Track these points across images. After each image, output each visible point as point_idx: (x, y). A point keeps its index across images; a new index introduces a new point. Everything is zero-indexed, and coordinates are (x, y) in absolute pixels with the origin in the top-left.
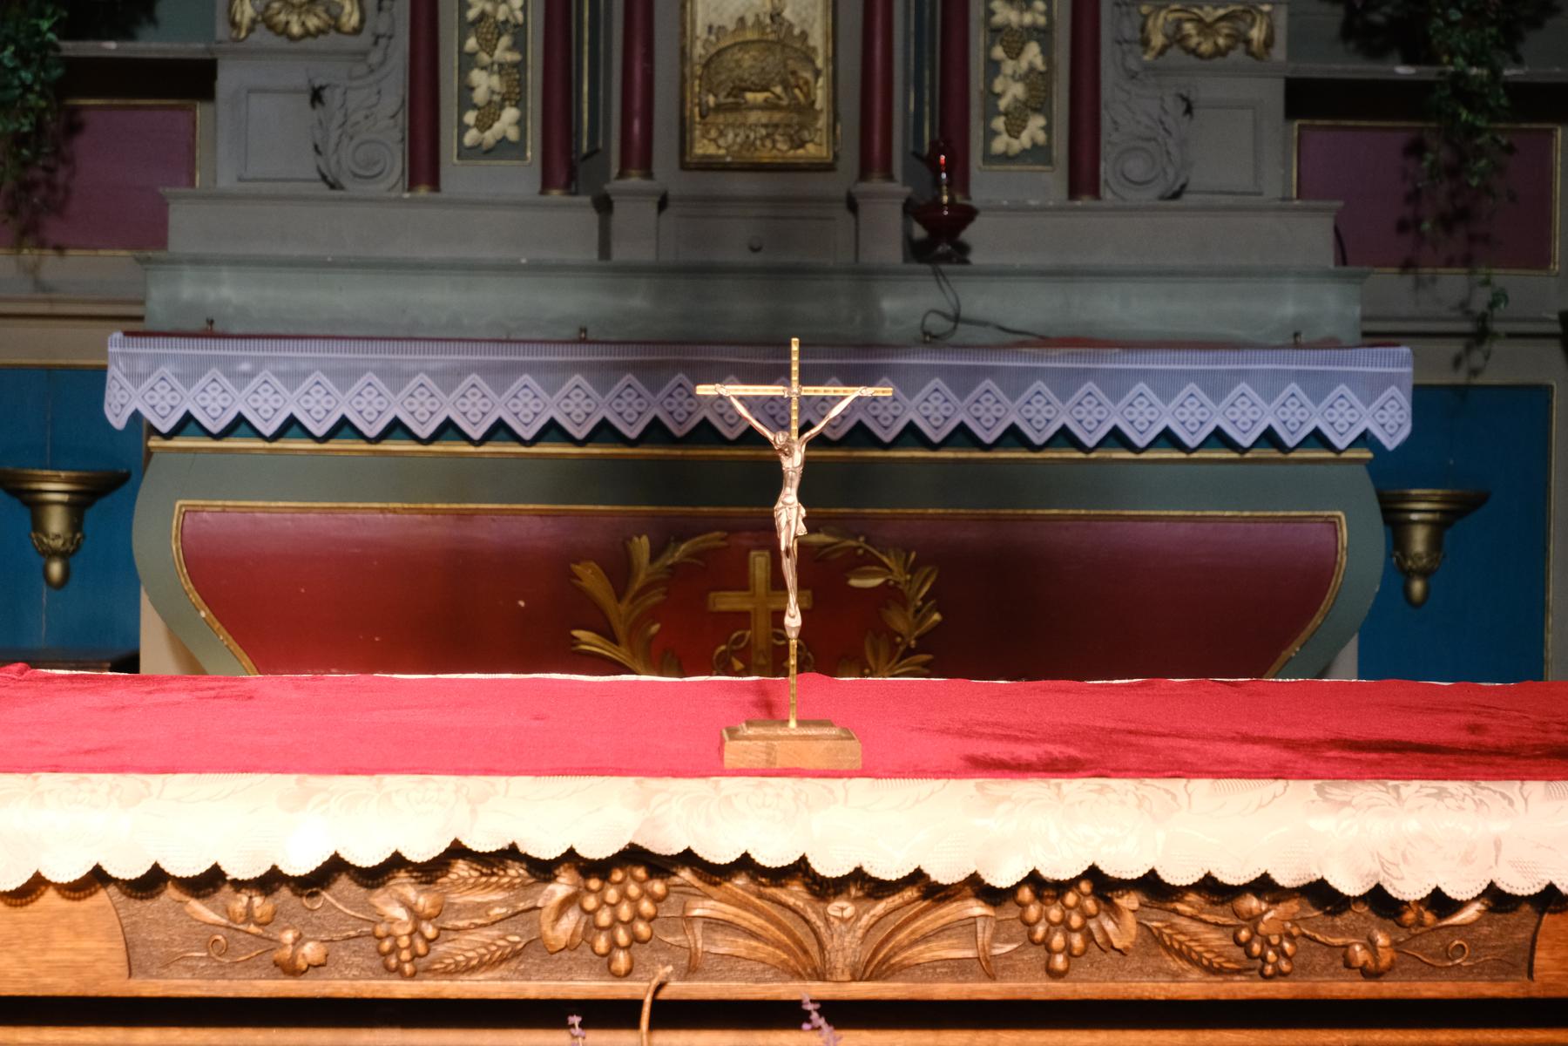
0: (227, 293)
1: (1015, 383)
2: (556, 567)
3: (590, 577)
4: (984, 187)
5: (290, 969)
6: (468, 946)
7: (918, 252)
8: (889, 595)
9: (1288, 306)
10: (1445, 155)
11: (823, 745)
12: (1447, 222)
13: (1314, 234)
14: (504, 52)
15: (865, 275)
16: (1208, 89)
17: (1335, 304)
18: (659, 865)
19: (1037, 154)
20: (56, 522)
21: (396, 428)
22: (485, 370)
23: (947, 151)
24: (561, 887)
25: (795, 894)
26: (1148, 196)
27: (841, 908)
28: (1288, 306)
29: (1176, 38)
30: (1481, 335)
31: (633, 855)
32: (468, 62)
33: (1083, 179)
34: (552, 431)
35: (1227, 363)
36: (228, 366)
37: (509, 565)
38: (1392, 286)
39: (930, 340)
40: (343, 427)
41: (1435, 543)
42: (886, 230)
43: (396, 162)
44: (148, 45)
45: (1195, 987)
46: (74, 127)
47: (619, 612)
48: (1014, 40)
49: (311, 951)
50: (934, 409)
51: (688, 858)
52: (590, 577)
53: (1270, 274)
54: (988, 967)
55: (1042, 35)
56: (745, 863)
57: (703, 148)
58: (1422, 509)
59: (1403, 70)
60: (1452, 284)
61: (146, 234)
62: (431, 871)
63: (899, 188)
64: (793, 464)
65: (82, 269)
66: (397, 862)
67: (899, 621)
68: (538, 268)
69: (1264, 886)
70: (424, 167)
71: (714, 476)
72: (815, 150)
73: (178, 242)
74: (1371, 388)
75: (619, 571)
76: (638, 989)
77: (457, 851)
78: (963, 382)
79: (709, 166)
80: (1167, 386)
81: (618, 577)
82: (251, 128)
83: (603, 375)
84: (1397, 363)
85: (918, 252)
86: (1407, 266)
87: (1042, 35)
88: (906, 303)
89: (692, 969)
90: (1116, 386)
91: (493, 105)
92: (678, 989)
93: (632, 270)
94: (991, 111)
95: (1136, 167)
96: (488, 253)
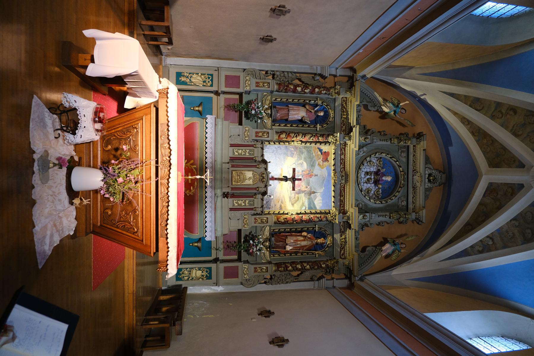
0: (219, 127)
1: (211, 202)
2: (193, 158)
3: (192, 162)
4: (230, 200)
5: (161, 137)
6: (163, 151)
7: (224, 193)
8: (190, 190)
9: (219, 229)
10: (234, 245)
11: (180, 180)
12: (228, 246)
13: (226, 232)
14: (243, 153)
15: (222, 188)
16: (240, 221)
17: (219, 234)
18: (170, 166)
19: (234, 205)
20: (197, 109)
21: (206, 148)
22: (212, 152)
23: (233, 196)
24: (168, 159)
25: (167, 177)
26: (230, 216)
27: (166, 181)
28: (219, 229)
29: (245, 218)
30: (217, 250)
31: (171, 164)
32: (242, 150)
33: (231, 209)
34: (206, 158)
35: (213, 223)
36: (212, 127)
37: (193, 154)
38: (221, 240)
39: (215, 194)
40: (206, 153)
41: (196, 246)
42: (226, 190)
43: (232, 143)
44: (244, 119)
45: (160, 210)
46: (236, 112)
47: (188, 164)
48: (245, 202)
49: (162, 138)
50: (208, 194)
51: (170, 169)
52: (192, 162)
53: (222, 228)
54: (161, 193)
55: (245, 205)
56: (170, 173)
57: (234, 172)
58: (199, 244)
59: (242, 240)
60: (221, 246)
61: (226, 119)
62: (169, 148)
63: (230, 191)
64: (202, 177)
65: (222, 112)
66: (170, 145)
67: (188, 191)
68: (222, 156)
69: (168, 215)
70: (232, 145)
71: (202, 170)
72: (234, 183)
73: (224, 122)
74: (211, 236)
75: (193, 164)
76: (159, 164)
77: (171, 150)
78: (211, 197)
79: (232, 173)
80: (211, 217)
81: (193, 164)
82: (236, 129)
83: (211, 163)
84: (213, 239)
85: (224, 193)
86: (223, 242)
87: (245, 205)
88: (219, 192)
89: (161, 169)
90: (211, 212)
91: (239, 152)
92: (159, 168)
93: (222, 165)
94: (238, 200)
95: (233, 215)
96: (223, 152)
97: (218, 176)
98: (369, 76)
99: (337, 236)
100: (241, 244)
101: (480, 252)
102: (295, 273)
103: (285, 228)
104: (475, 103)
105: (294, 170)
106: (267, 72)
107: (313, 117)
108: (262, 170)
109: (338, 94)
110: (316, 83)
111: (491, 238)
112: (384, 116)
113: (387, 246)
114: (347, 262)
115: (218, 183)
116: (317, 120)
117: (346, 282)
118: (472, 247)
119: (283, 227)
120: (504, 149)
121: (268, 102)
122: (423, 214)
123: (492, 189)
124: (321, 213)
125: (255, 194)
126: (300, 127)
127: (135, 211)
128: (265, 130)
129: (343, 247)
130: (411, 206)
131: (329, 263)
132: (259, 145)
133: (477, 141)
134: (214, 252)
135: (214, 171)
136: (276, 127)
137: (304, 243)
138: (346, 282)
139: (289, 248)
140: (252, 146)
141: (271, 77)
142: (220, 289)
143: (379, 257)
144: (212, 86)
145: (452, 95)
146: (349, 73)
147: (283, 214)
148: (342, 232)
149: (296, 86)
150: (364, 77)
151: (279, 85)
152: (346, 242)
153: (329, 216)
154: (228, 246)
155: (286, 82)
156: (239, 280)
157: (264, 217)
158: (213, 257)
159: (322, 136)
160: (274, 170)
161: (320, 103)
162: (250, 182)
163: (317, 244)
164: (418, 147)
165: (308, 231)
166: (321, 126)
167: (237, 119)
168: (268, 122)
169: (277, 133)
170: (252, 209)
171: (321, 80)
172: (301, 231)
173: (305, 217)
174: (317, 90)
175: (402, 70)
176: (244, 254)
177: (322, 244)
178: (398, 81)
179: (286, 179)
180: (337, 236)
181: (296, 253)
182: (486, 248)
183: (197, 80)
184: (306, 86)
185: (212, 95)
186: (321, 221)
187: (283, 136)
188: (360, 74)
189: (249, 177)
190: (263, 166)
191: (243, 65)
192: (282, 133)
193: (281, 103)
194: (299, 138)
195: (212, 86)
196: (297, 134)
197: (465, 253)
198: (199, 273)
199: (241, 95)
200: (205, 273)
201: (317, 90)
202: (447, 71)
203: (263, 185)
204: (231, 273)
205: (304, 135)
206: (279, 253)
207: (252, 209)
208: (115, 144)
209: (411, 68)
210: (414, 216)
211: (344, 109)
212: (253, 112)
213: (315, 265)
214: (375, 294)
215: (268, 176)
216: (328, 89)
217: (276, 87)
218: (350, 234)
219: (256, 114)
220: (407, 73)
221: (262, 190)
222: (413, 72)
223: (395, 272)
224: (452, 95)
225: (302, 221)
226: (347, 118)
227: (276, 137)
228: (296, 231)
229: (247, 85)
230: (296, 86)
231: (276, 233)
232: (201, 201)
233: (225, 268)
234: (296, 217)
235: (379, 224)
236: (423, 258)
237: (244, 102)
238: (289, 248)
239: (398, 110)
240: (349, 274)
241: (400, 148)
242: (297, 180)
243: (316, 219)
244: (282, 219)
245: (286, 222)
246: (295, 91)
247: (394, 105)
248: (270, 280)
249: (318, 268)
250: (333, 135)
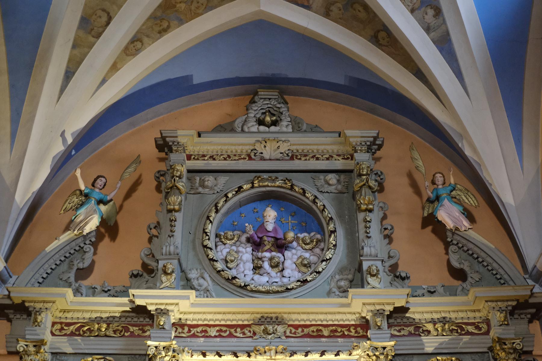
101: (438, 12)
112: (109, 229)
113: (442, 215)
114: (497, 317)
118: (428, 29)
129: (459, 329)
130: (339, 164)
133: (181, 22)
145: (69, 75)
148: (418, 330)
152: (444, 321)
164: (190, 149)
178: (23, 196)
197: (444, 44)
210: (362, 157)
211: (81, 330)
218: (421, 310)
224: (69, 75)
226: (109, 321)
236: (464, 135)
241: (192, 190)
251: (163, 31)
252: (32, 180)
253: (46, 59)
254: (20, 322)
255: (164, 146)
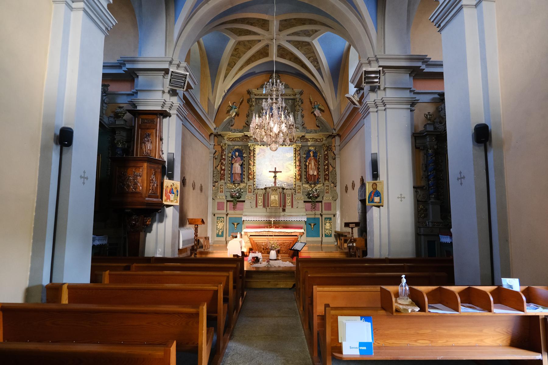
0: (247, 214)
4: (287, 207)
13: (304, 210)
28: (302, 214)
33: (292, 207)
42: (281, 210)
60: (314, 212)
65: (238, 212)
70: (256, 206)
81: (269, 224)
82: (247, 205)
84: (306, 217)
88: (282, 214)
91: (260, 202)
97: (274, 214)
98: (215, 126)
99: (309, 144)
100: (312, 200)
101: (318, 63)
102: (331, 169)
103: (303, 174)
104: (231, 65)
105: (270, 172)
106: (214, 186)
107: (239, 158)
108: (270, 190)
109: (225, 144)
110: (219, 158)
111: (310, 58)
112: (237, 114)
113: (315, 113)
114: (324, 138)
115: (277, 214)
116: (241, 156)
117: (337, 138)
118: (315, 67)
119: (304, 177)
120: (258, 52)
121: (231, 185)
122: (296, 90)
123: (280, 55)
124: (295, 153)
125: (284, 193)
126: (245, 166)
127: (284, 243)
128: (247, 187)
129: (316, 140)
130: (292, 97)
131: (325, 149)
132: (256, 191)
133: (253, 62)
134: (317, 216)
135: (270, 216)
136: (246, 180)
137: (313, 164)
138: (337, 138)
139: (315, 173)
140: (257, 195)
141: (217, 183)
142: (338, 213)
143: (322, 118)
144: (223, 218)
145: (225, 77)
146: (213, 136)
147: (296, 176)
148: (307, 140)
149: (222, 169)
150: (215, 129)
151: (221, 179)
152: (313, 138)
153: (298, 149)
154: (314, 208)
155: (219, 175)
156: (332, 202)
157: (297, 188)
158: (320, 216)
159: (250, 153)
160: (271, 184)
161: (230, 155)
162: (277, 196)
163: (313, 156)
164: (256, 93)
165: (306, 162)
166: (245, 154)
167: (241, 203)
168: (242, 185)
169: (249, 180)
170: (292, 195)
171: (217, 154)
172: (306, 165)
173: (298, 163)
174: (224, 157)
175: (210, 105)
176: (317, 200)
177: (314, 153)
178: (216, 107)
179: (275, 177)
180: (309, 144)
181: (318, 168)
182: (315, 61)
183: (220, 225)
184: (222, 164)
185: (228, 217)
186: (300, 154)
187: (250, 177)
188: (213, 131)
189: (274, 197)
190: (268, 190)
191: (210, 199)
192: (249, 178)
193: (231, 177)
194: (251, 167)
195: (223, 218)
196: (249, 169)
197: (319, 70)
198: (328, 224)
199: (228, 201)
200: (328, 221)
201: (224, 157)
202: (211, 80)
203: (278, 190)
204: (328, 207)
205: (249, 164)
206: (318, 178)
207: (292, 195)
208: (262, 249)
209: (209, 99)
210: (298, 96)
211: (233, 140)
212: (237, 194)
213: (326, 157)
214: (340, 125)
215: (273, 187)
216: (223, 150)
217: (222, 181)
218: (308, 136)
219: (238, 192)
220: (212, 102)
221: (281, 190)
222: (211, 98)
223: (332, 108)
224: (225, 77)
225: (300, 165)
226: (239, 138)
227: (251, 181)
228: (306, 168)
229: (222, 197)
230: (222, 169)
231: (307, 180)
232: (286, 223)
233: (325, 210)
234: (298, 169)
235: (303, 116)
236: (323, 91)
237: (232, 199)
238: (315, 173)
239: (234, 107)
240: (332, 136)
241: (256, 104)
242: (275, 164)
243: (299, 157)
244: (298, 177)
245: (300, 175)
246: (224, 170)
247: (231, 110)
248: (335, 184)
249: (328, 156)
250: (249, 147)
251: (248, 65)
252: (219, 101)
253: (220, 72)
254: (220, 138)
255: (249, 92)
